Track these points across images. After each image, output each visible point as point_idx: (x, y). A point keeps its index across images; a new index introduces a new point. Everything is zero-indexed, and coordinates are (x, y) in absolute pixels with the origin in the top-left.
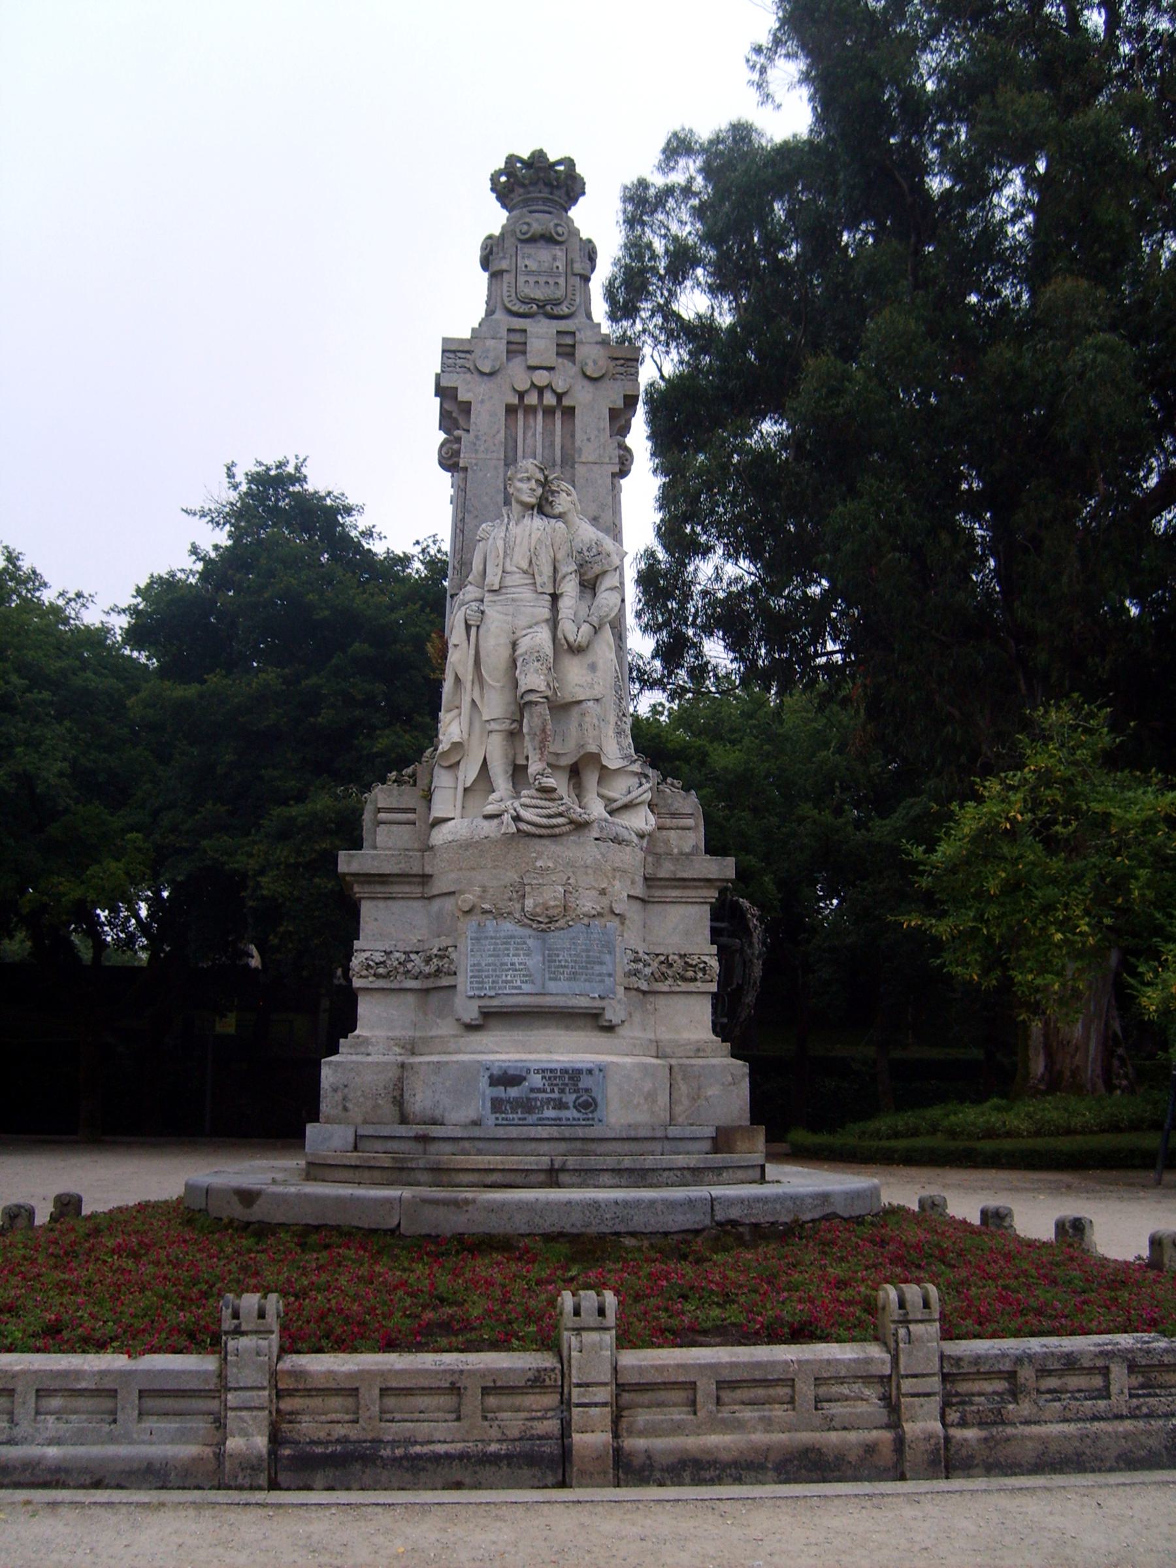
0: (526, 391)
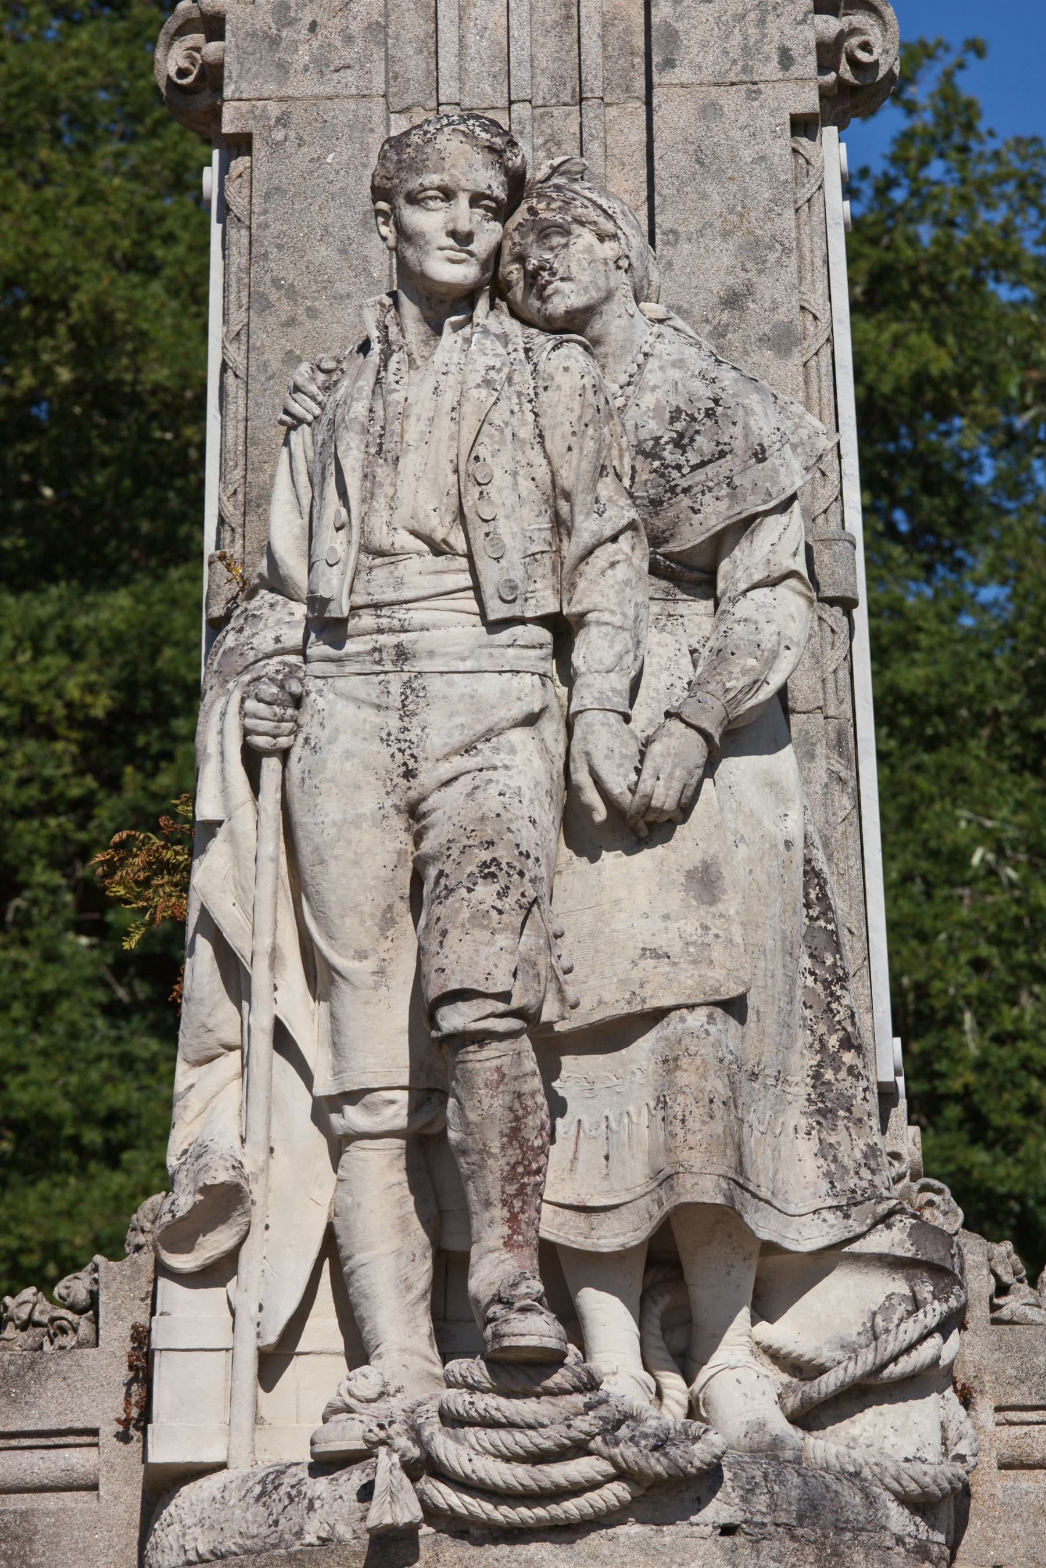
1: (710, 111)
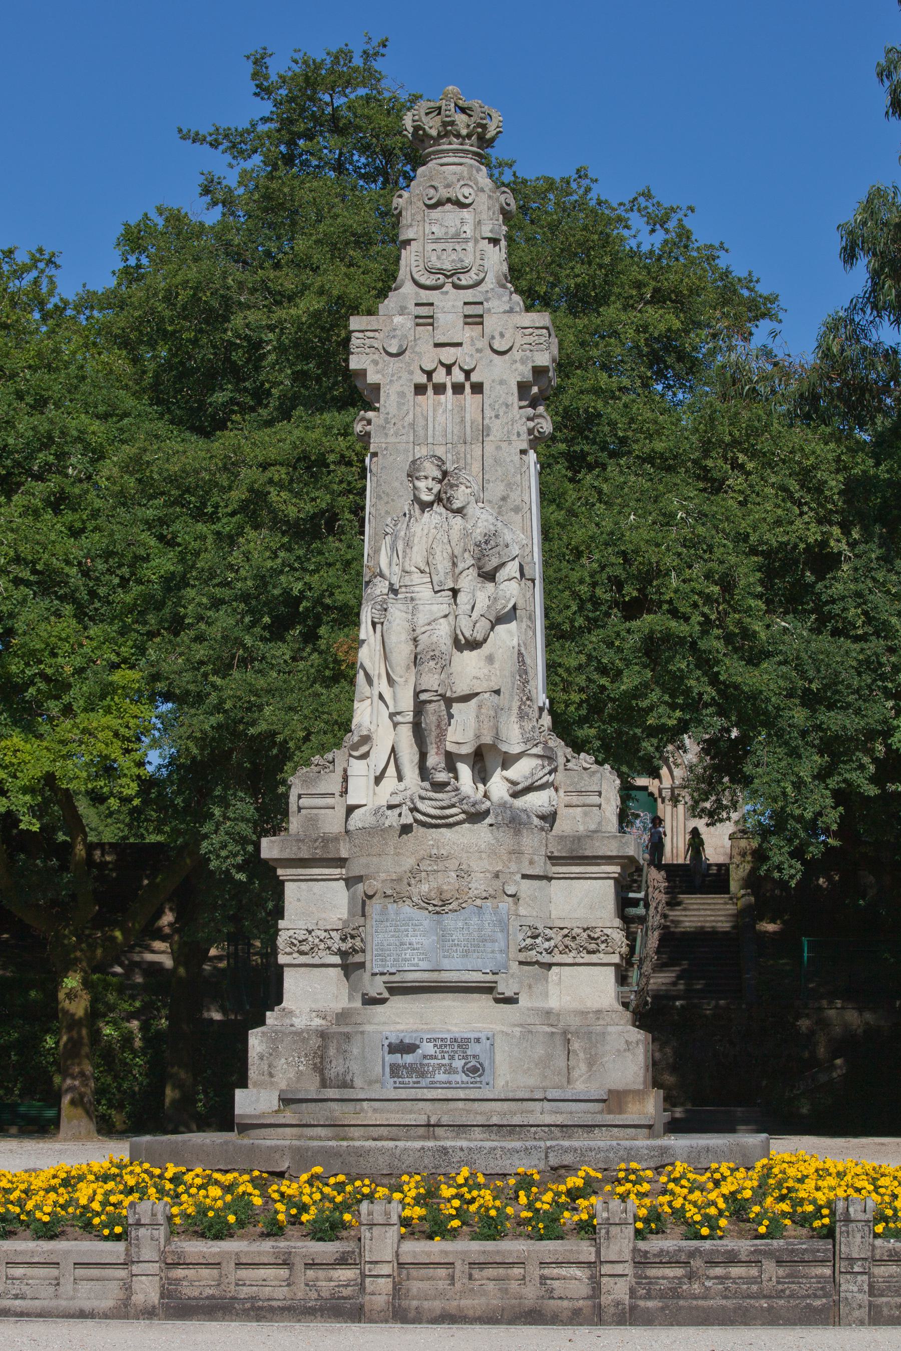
0: (435, 370)
1: (498, 448)
